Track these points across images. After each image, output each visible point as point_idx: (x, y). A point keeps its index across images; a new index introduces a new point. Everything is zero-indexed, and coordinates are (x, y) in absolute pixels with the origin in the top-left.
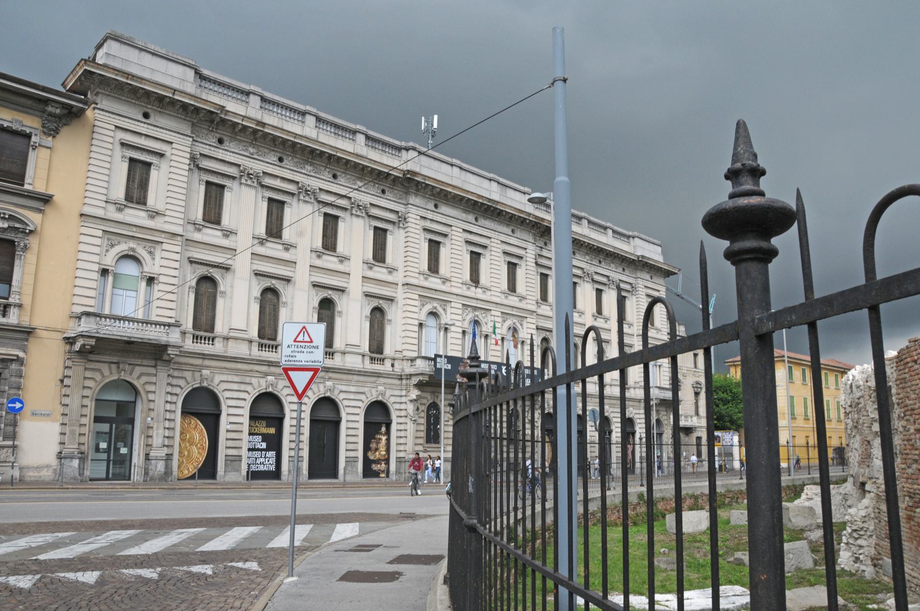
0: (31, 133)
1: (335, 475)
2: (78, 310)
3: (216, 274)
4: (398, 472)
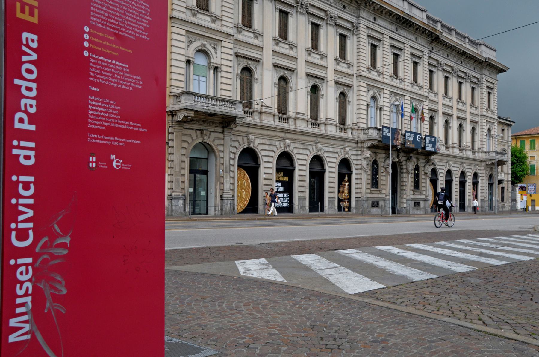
1: (322, 210)
3: (287, 74)
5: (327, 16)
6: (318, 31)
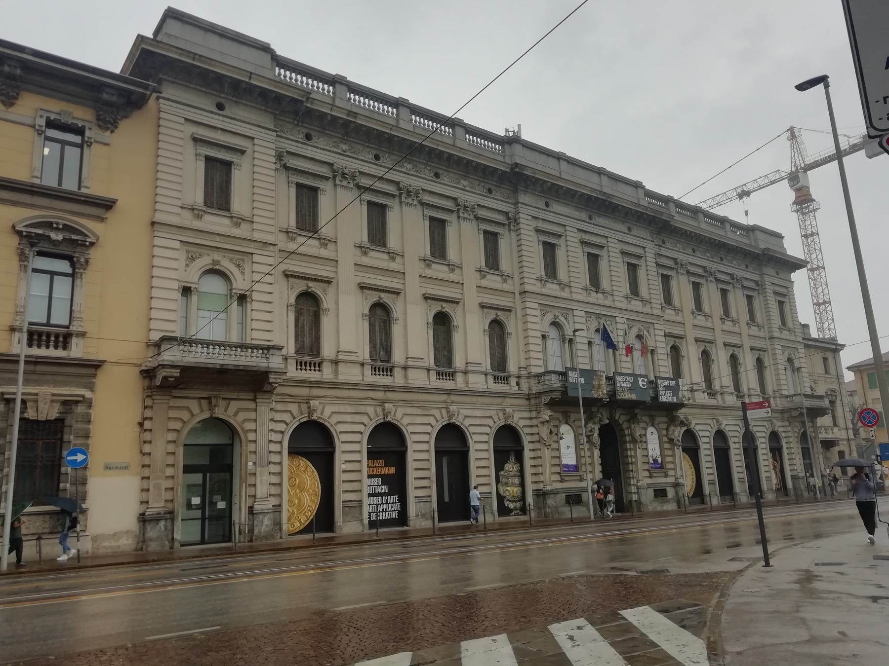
0: (84, 127)
2: (155, 336)
5: (334, 171)
6: (496, 243)
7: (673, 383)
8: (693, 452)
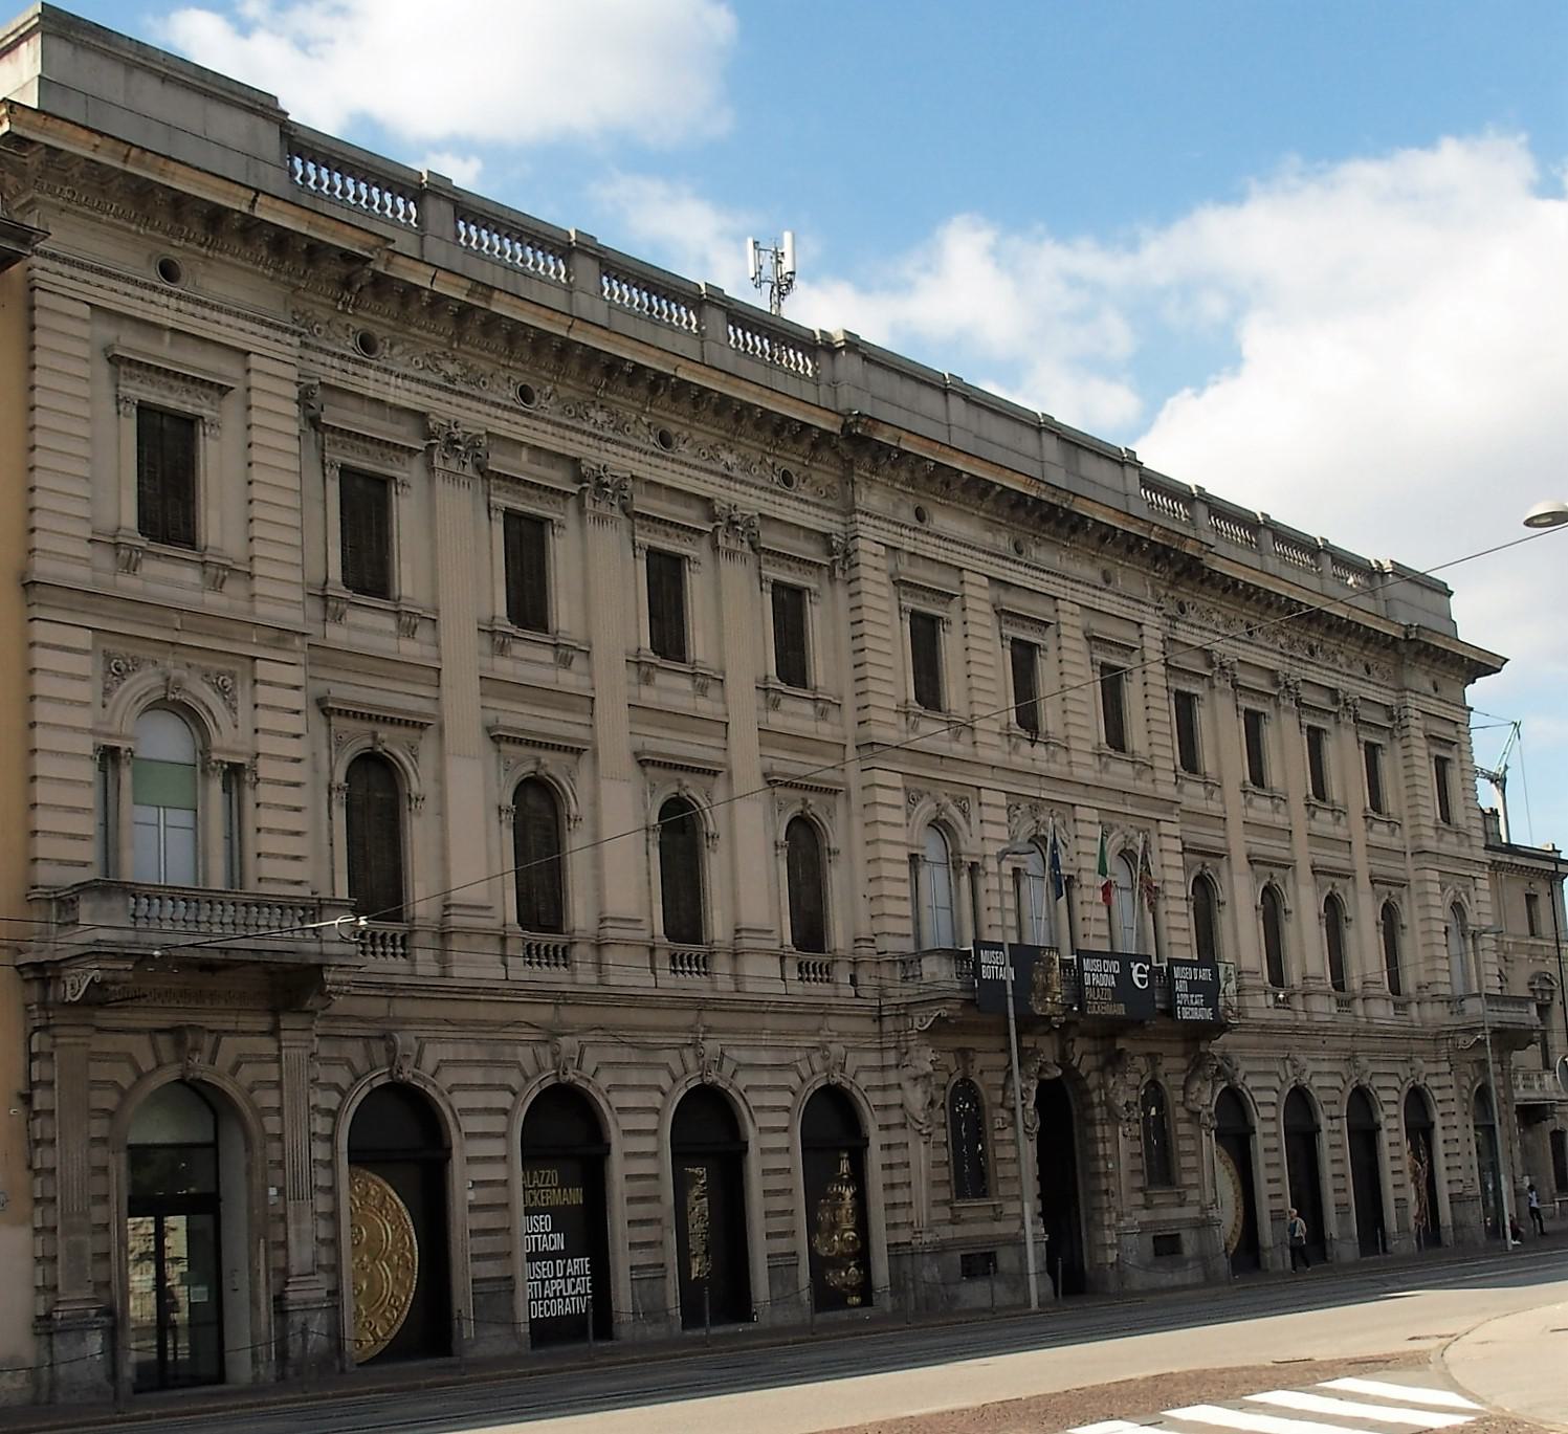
3: (392, 741)
4: (897, 1285)
7: (1205, 974)
8: (1237, 1140)
